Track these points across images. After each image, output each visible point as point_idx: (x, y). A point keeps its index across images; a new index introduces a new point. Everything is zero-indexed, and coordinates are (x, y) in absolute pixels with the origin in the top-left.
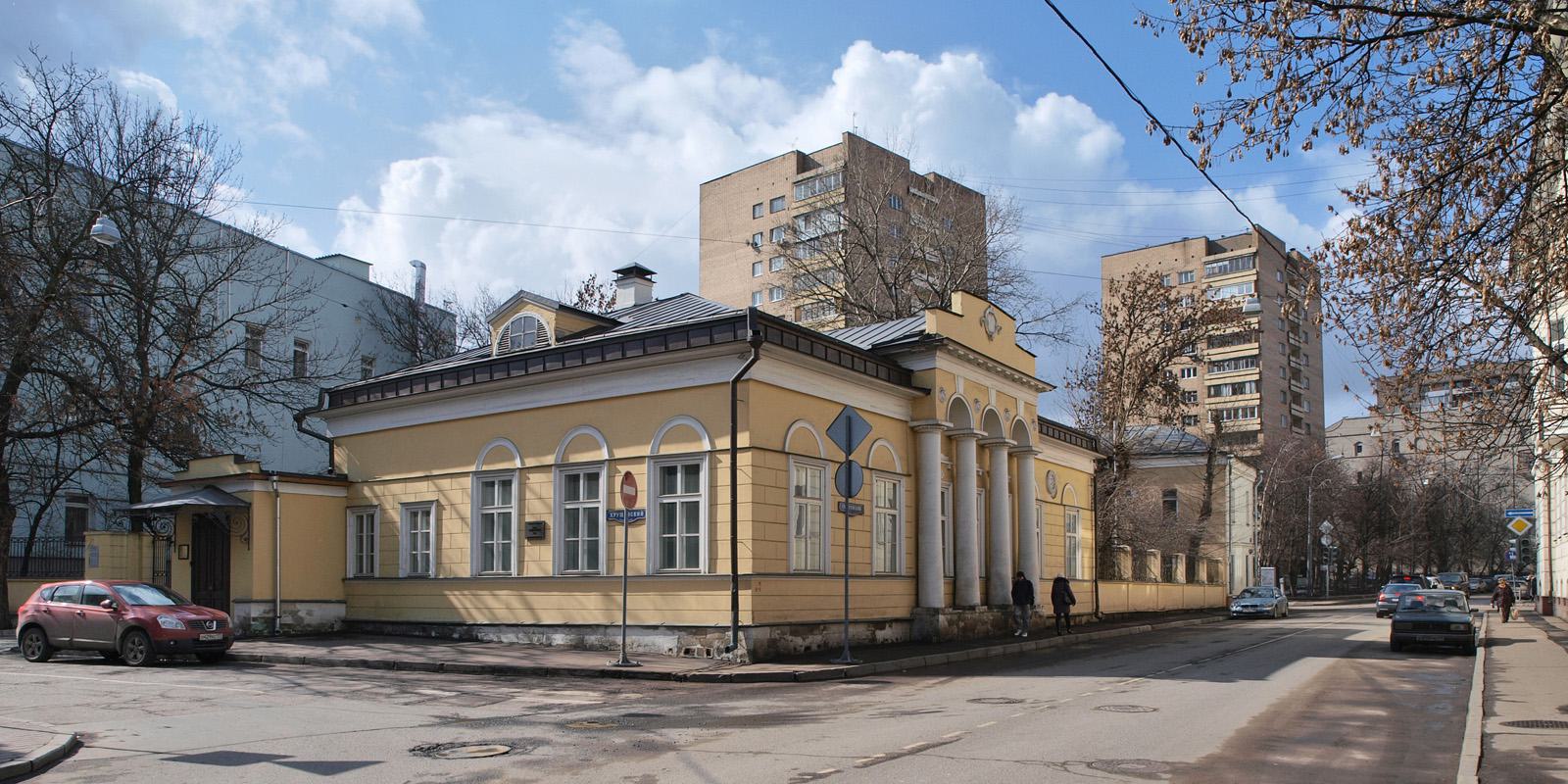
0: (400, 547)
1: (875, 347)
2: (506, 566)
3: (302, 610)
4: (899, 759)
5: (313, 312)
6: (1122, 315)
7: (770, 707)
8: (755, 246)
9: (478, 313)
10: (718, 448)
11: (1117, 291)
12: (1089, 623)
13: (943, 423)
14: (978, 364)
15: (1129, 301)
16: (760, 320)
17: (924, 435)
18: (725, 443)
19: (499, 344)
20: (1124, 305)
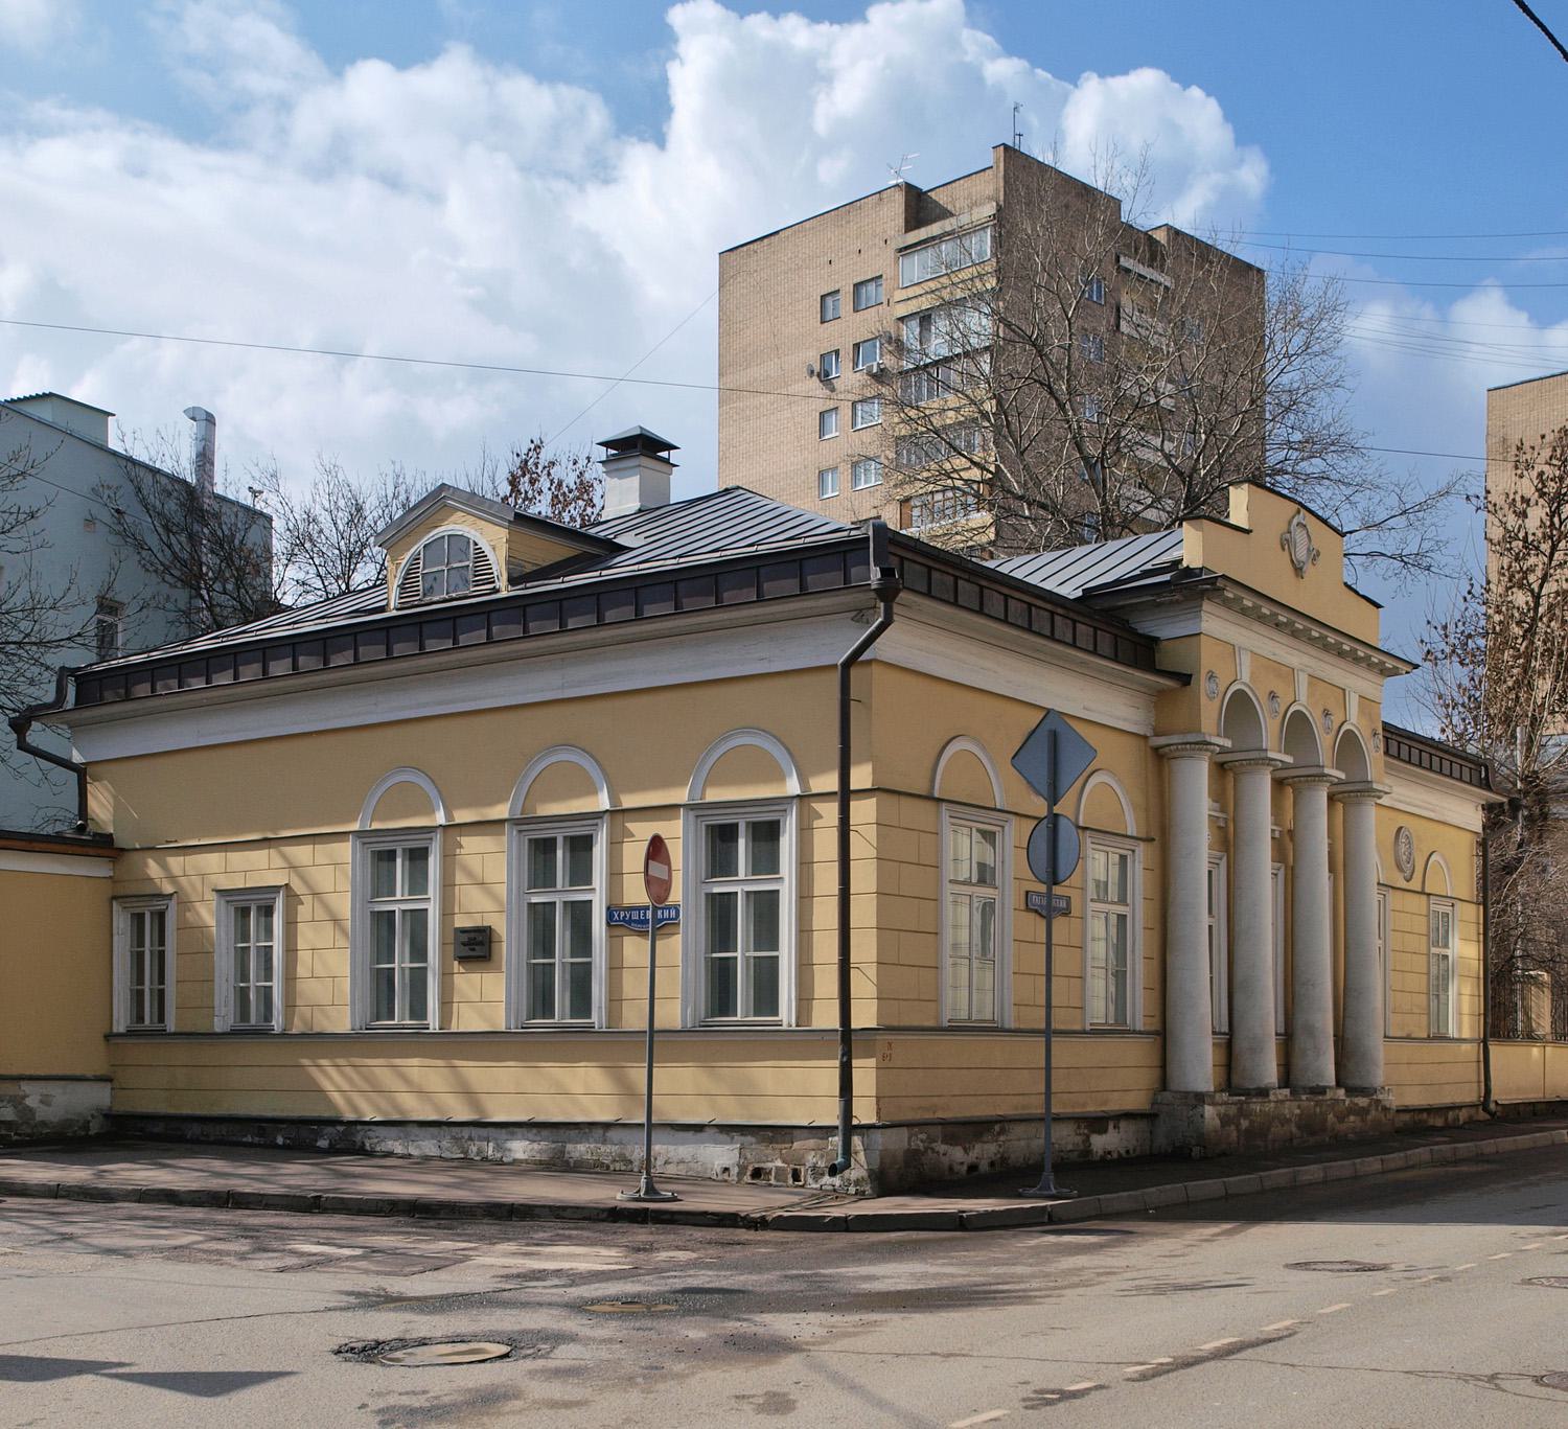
0: (217, 974)
1: (1089, 595)
2: (418, 1009)
3: (33, 1095)
4: (1197, 1367)
5: (33, 516)
6: (1537, 514)
7: (935, 1276)
8: (824, 377)
9: (317, 511)
10: (814, 791)
11: (1529, 466)
12: (1471, 1121)
13: (1215, 740)
14: (1278, 625)
15: (1552, 487)
16: (892, 549)
17: (1178, 761)
18: (829, 782)
19: (402, 587)
20: (1542, 495)
